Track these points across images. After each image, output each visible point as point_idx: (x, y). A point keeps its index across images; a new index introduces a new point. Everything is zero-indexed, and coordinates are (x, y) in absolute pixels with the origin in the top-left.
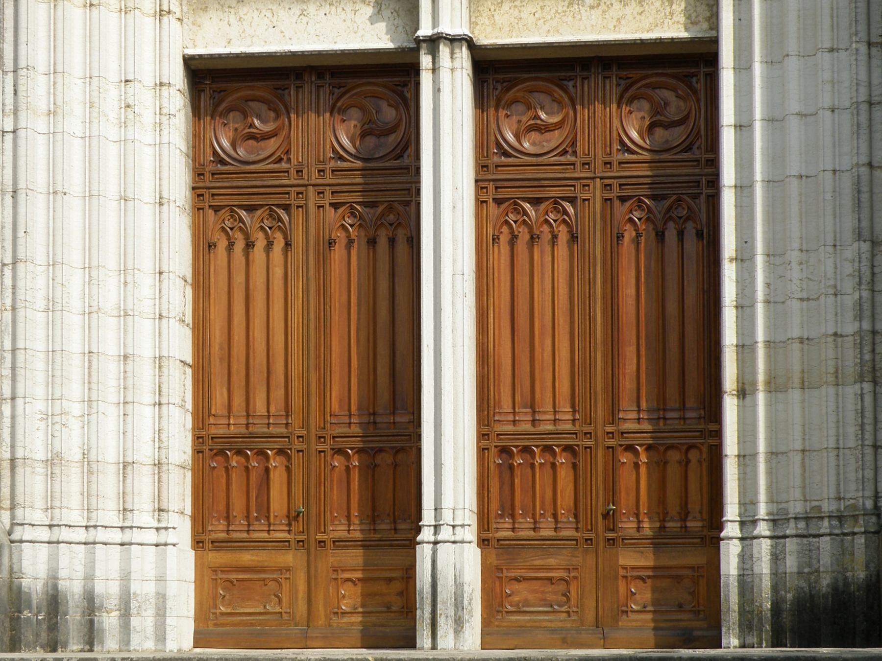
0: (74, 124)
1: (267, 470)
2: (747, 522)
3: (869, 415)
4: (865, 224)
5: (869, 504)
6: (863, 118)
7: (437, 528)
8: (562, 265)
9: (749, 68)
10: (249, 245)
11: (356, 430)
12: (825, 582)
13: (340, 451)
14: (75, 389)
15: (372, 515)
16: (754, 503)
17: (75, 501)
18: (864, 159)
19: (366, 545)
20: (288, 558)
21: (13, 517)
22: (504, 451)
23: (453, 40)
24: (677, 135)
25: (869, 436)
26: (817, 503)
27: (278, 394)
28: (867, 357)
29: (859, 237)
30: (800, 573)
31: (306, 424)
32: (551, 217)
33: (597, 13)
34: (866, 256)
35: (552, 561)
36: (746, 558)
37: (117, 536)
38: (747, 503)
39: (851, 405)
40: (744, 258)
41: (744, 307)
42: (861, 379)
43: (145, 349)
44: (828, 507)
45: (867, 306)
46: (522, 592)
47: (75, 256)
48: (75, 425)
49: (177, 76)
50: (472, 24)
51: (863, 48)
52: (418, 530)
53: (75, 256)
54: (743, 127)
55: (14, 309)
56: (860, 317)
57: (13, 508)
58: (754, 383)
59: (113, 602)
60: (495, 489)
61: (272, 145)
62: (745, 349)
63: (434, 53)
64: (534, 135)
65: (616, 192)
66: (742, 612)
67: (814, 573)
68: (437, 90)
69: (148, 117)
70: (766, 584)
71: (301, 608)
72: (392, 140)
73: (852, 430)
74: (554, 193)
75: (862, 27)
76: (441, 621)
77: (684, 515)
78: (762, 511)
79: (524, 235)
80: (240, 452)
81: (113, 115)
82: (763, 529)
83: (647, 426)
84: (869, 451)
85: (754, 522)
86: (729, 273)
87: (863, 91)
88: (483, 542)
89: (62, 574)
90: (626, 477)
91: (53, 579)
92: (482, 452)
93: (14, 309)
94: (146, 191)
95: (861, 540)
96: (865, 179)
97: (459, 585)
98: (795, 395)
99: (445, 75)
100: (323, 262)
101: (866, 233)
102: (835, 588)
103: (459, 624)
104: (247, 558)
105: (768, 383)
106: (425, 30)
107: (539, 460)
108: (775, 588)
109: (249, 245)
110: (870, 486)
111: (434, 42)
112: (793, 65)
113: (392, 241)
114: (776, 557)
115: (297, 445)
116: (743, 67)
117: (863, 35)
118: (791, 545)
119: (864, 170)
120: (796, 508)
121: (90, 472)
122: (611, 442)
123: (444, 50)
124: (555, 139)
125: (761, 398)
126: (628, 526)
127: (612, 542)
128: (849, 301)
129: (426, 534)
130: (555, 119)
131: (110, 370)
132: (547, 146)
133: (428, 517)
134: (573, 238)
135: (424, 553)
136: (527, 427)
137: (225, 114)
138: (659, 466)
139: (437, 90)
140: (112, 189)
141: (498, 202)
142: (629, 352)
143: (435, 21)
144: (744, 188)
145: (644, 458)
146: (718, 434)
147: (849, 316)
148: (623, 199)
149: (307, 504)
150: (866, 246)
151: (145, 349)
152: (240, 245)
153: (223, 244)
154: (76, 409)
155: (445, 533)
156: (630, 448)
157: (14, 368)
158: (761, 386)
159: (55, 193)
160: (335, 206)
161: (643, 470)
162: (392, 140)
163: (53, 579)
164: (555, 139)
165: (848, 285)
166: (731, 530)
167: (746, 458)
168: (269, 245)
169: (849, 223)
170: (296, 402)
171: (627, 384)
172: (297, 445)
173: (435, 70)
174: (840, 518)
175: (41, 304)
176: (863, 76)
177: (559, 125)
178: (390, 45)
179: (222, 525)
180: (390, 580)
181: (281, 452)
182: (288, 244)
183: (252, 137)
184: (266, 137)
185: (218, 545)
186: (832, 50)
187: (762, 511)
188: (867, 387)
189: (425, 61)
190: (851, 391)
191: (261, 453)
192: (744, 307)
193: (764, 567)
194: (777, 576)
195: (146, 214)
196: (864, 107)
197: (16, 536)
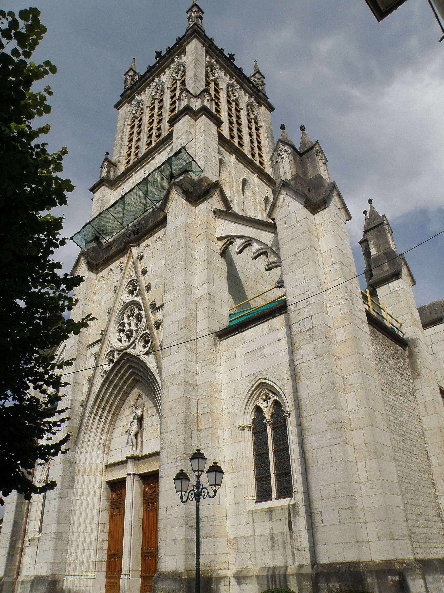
49: (104, 485)
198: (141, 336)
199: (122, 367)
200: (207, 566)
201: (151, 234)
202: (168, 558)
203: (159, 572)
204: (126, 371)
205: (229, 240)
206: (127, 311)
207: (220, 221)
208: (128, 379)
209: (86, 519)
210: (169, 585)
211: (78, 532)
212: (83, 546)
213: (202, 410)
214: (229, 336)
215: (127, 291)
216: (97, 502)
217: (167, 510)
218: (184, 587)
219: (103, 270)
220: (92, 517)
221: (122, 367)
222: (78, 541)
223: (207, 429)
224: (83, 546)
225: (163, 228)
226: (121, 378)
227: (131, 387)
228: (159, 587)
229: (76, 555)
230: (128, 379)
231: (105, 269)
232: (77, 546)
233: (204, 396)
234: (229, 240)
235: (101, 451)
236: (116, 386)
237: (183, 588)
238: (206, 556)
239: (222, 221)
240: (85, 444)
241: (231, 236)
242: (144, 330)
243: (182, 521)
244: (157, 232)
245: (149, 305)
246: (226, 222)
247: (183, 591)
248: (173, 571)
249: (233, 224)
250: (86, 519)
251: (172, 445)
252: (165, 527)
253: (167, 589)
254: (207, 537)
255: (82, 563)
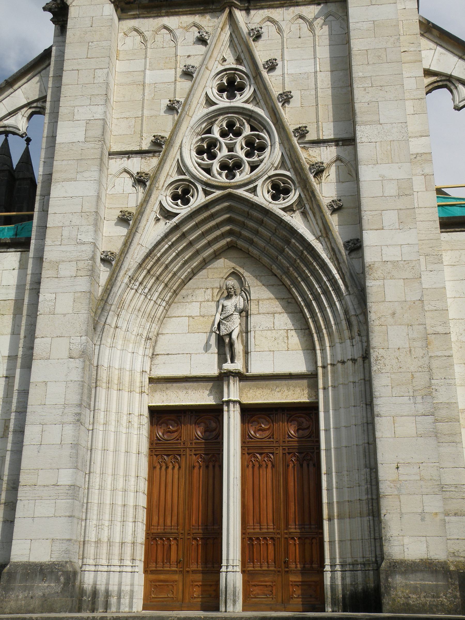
0: (112, 428)
1: (170, 545)
2: (333, 565)
3: (372, 527)
4: (368, 462)
5: (374, 559)
6: (365, 428)
7: (227, 566)
8: (270, 475)
9: (328, 411)
10: (167, 467)
11: (200, 531)
12: (360, 587)
13: (195, 539)
14: (107, 517)
15: (205, 562)
16: (335, 558)
17: (104, 556)
18: (366, 441)
19: (203, 572)
20: (176, 577)
21: (83, 562)
22: (250, 539)
23: (234, 402)
24: (307, 432)
25: (372, 535)
26: (239, 347)
27: (175, 518)
28: (370, 508)
29: (366, 467)
30: (351, 584)
31: (184, 529)
32: (266, 459)
33: (280, 393)
34: (368, 473)
35: (267, 579)
36: (333, 578)
37: (118, 569)
38: (333, 559)
39: (366, 524)
40: (329, 473)
41: (329, 490)
42: (369, 515)
43: (131, 502)
44: (360, 560)
45: (369, 490)
46: (256, 590)
47: (110, 471)
48: (106, 529)
49: (146, 412)
50: (240, 397)
51: (364, 406)
52: (221, 567)
53: (110, 471)
54: (327, 431)
55: (88, 489)
56: (367, 494)
57: (83, 559)
58: (333, 516)
59: (115, 593)
60: (247, 552)
61: (176, 434)
62: (330, 504)
63: (228, 406)
64: (260, 432)
65: (287, 451)
66: (332, 598)
67: (354, 584)
68: (229, 418)
69: (136, 425)
70: (340, 588)
71: (180, 596)
72: (214, 433)
73: (367, 533)
74: (267, 451)
75: (364, 399)
76: (228, 601)
77: (312, 562)
78: (338, 561)
79: (257, 465)
80: (161, 539)
81: (125, 425)
82: (338, 568)
83: (298, 531)
84: (373, 540)
85: (335, 565)
86: (324, 478)
87: (365, 419)
88: (243, 572)
89: (98, 583)
90: (292, 548)
91: (95, 584)
92: (243, 539)
93: (88, 489)
94: (134, 449)
95: (371, 573)
96: (367, 448)
97: (235, 588)
98: (347, 520)
99: (232, 413)
100: (191, 474)
101: (368, 466)
102: (363, 589)
103: (234, 602)
104: (162, 577)
105: (338, 516)
106: (225, 399)
107: (262, 542)
108: (343, 590)
109: (167, 467)
110: (373, 553)
111: (228, 402)
112: (342, 410)
113: (214, 466)
114: (343, 578)
115: (181, 536)
116: (327, 411)
117: (364, 402)
118: (348, 574)
119: (366, 445)
120: (349, 560)
121: (110, 546)
122: (287, 536)
123: (231, 405)
124: (267, 433)
125: (336, 521)
126: (292, 566)
127: (287, 572)
128: (364, 488)
129: (224, 569)
130: (267, 427)
131: (119, 510)
132: (264, 436)
133: (224, 563)
134: (273, 466)
135: (223, 575)
136: (258, 530)
137: (160, 425)
138: (302, 545)
139: (229, 418)
140: (123, 449)
141: (249, 454)
142: (292, 504)
143: (229, 397)
144: (328, 450)
145: (297, 542)
146: (322, 534)
147: (364, 493)
148: (289, 453)
149: (183, 557)
150: (368, 470)
151: (131, 502)
152: (164, 467)
153: (158, 467)
154: (107, 523)
155: (230, 569)
156: (293, 538)
157: (87, 509)
158: (336, 517)
159: (105, 450)
160: (196, 455)
161: (297, 546)
162: (214, 433)
163: (95, 584)
164: (267, 433)
165: (363, 483)
166: (328, 568)
167: (332, 542)
168: (174, 468)
169: (362, 462)
170: (181, 521)
171: (292, 516)
172: (181, 536)
173: (228, 411)
174: (364, 564)
175: (97, 487)
176: (365, 415)
177: (268, 429)
178: (214, 403)
179: (154, 565)
180: (211, 585)
181: (175, 539)
182: (180, 467)
183: (169, 432)
184: (174, 432)
185: (152, 572)
186: (354, 406)
187: (338, 561)
188: (371, 518)
189: (225, 408)
190: (366, 519)
191: (168, 539)
192: (329, 490)
193: (339, 582)
194: (344, 585)
195: (133, 458)
196: (366, 425)
197: (83, 569)
198: (269, 177)
199: (212, 217)
200: (459, 556)
201: (285, 3)
202: (406, 540)
203: (389, 559)
204: (218, 226)
205: (441, 81)
206: (222, 120)
207: (426, 43)
208: (216, 240)
209: (115, 467)
210: (421, 580)
211: (101, 488)
212: (124, 515)
213: (433, 327)
214: (457, 230)
215: (216, 82)
216: (135, 439)
217: (398, 468)
218: (457, 583)
219: (139, 18)
220: (127, 463)
221: (212, 217)
222: (100, 504)
223: (445, 358)
224: (124, 515)
225: (314, 4)
226: (203, 235)
227: (216, 256)
228: (398, 582)
229: (99, 527)
230: (216, 240)
231: (144, 17)
232: (100, 513)
233: (435, 308)
234: (441, 81)
235: (141, 352)
236: (191, 244)
237: (454, 584)
238: (456, 541)
239: (432, 45)
240: (120, 333)
241: (451, 76)
242: (276, 169)
243: (436, 487)
244: (298, 5)
245: (47, 116)
246: (439, 49)
247: (455, 588)
248: (422, 559)
249: (456, 59)
250: (115, 467)
251: (400, 370)
252: (396, 493)
253: (418, 585)
254: (456, 514)
255: (110, 543)
